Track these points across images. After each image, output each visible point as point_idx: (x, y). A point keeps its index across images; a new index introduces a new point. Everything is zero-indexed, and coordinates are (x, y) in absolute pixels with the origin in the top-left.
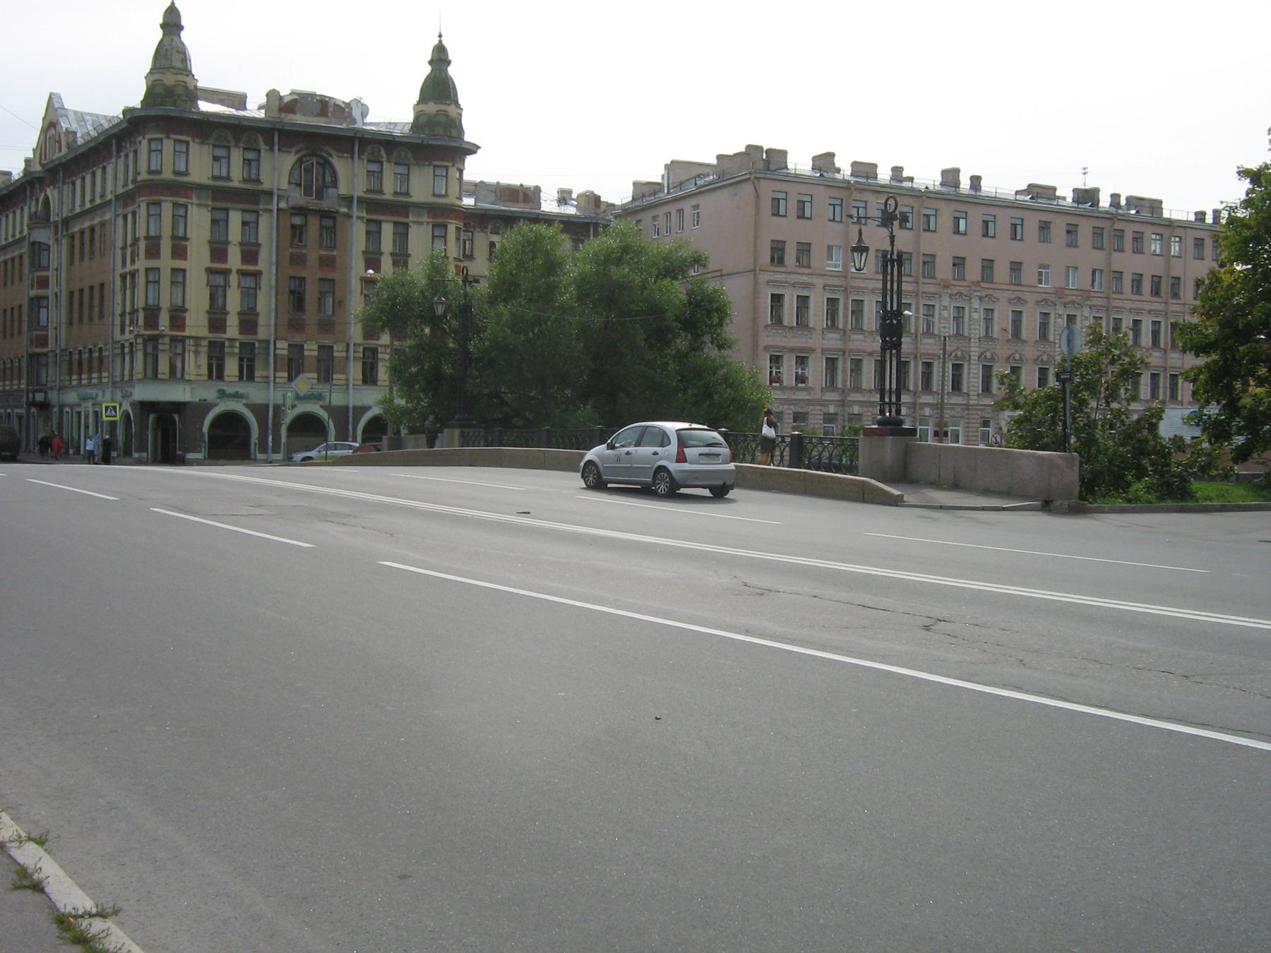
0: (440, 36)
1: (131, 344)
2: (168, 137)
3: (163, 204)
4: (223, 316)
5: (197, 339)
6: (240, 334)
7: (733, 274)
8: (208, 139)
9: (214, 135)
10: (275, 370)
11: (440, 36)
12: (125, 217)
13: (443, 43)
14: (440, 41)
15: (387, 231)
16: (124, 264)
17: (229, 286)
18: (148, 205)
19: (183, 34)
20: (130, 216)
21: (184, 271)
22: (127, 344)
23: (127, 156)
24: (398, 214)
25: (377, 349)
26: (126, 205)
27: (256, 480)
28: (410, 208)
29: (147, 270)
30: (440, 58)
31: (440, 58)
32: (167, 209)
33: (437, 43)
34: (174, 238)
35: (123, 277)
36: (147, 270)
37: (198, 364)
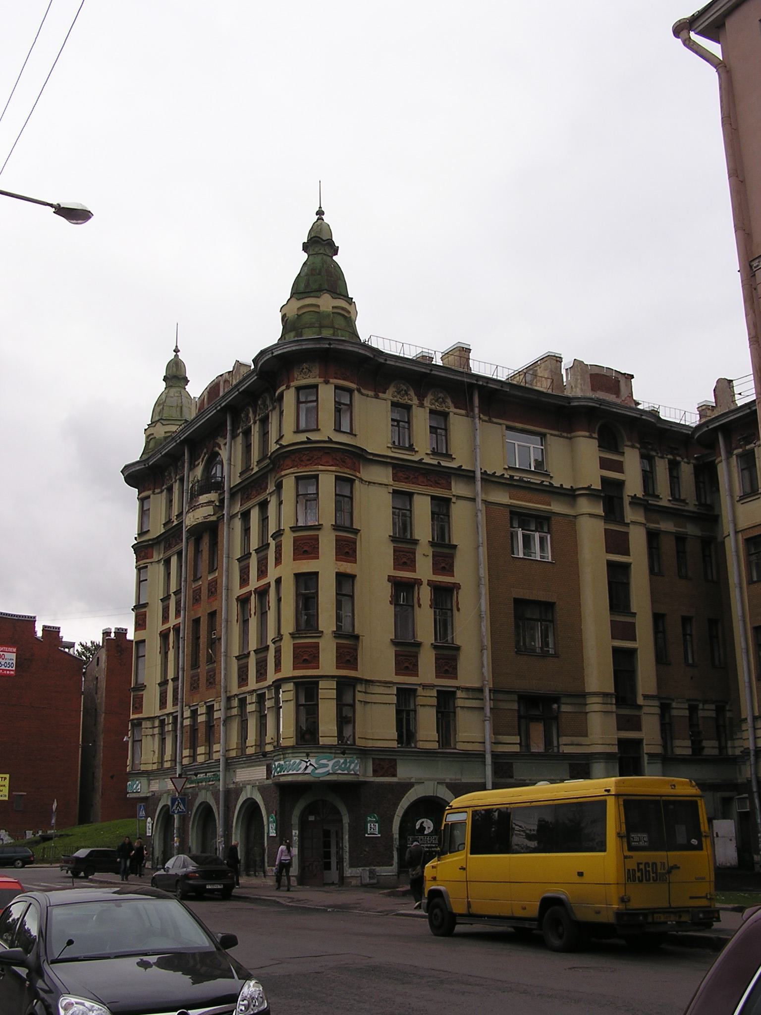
0: (176, 351)
2: (327, 382)
3: (322, 477)
4: (453, 653)
9: (391, 390)
12: (246, 516)
14: (177, 356)
16: (244, 581)
17: (420, 606)
18: (298, 479)
20: (255, 514)
21: (353, 577)
23: (247, 433)
24: (437, 484)
26: (246, 499)
28: (453, 478)
32: (327, 483)
35: (244, 601)
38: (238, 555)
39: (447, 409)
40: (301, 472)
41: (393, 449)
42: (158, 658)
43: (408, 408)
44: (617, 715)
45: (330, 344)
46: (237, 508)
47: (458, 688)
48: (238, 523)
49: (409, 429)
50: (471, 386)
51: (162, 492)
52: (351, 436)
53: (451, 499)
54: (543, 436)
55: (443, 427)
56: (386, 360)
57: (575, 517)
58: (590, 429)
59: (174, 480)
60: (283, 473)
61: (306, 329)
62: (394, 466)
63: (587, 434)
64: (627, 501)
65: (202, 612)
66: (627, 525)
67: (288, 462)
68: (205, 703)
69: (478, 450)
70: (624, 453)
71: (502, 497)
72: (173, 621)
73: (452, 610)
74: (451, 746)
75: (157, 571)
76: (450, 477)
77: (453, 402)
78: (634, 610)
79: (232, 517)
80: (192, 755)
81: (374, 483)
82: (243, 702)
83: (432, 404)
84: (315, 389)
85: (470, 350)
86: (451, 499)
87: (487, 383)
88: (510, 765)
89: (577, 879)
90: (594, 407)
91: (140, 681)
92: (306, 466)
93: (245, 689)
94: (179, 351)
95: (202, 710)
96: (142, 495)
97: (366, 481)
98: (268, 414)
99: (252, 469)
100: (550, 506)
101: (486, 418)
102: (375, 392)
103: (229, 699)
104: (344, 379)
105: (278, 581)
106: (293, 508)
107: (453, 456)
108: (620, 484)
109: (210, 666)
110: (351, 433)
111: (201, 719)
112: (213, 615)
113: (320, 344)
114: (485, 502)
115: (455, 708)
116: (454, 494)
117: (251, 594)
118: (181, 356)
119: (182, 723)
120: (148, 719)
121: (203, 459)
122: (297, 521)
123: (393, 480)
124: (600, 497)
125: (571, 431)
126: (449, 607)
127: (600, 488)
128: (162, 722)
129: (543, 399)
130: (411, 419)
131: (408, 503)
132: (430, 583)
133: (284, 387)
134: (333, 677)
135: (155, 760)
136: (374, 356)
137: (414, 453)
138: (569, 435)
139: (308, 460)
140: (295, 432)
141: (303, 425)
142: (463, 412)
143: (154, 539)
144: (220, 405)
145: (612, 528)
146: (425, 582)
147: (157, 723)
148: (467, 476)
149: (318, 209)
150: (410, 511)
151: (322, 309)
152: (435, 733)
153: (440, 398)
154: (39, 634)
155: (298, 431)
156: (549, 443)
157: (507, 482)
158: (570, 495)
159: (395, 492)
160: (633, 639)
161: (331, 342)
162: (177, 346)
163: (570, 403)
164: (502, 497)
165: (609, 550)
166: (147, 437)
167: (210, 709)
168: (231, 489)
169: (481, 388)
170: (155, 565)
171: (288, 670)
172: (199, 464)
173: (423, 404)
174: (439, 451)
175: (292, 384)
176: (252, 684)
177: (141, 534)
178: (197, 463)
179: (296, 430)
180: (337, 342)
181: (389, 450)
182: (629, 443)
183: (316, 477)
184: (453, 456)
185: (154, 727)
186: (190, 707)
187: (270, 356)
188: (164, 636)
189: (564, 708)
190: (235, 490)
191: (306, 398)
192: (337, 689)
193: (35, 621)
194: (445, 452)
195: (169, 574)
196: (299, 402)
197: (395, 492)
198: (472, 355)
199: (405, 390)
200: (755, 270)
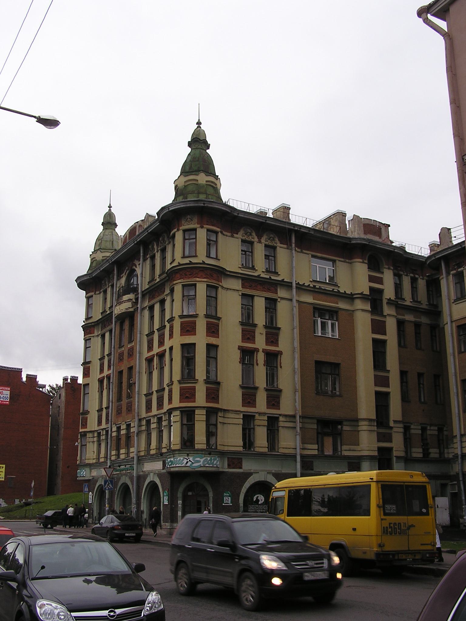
0: (110, 207)
2: (202, 227)
3: (198, 285)
4: (252, 391)
6: (267, 408)
8: (136, 565)
9: (242, 232)
10: (341, 445)
11: (110, 207)
12: (151, 308)
13: (112, 211)
14: (110, 210)
15: (260, 304)
16: (150, 348)
17: (257, 364)
18: (184, 286)
20: (157, 307)
21: (217, 347)
23: (153, 258)
24: (269, 290)
27: (199, 564)
32: (201, 289)
33: (108, 211)
35: (150, 360)
41: (242, 269)
42: (97, 395)
45: (204, 204)
46: (146, 304)
47: (280, 415)
48: (146, 313)
50: (290, 230)
51: (100, 293)
54: (334, 261)
57: (353, 311)
59: (107, 286)
60: (175, 282)
61: (190, 195)
62: (243, 279)
63: (361, 260)
64: (385, 302)
65: (124, 367)
66: (385, 316)
67: (178, 275)
68: (126, 422)
70: (383, 272)
71: (308, 299)
72: (106, 372)
73: (277, 367)
75: (97, 342)
76: (277, 286)
77: (279, 240)
79: (143, 309)
81: (230, 289)
82: (148, 422)
84: (195, 232)
85: (290, 208)
86: (277, 299)
87: (300, 228)
89: (353, 533)
91: (86, 409)
94: (111, 207)
95: (124, 427)
97: (225, 288)
98: (155, 254)
99: (156, 280)
101: (299, 250)
103: (140, 420)
104: (213, 225)
107: (279, 273)
108: (381, 292)
110: (217, 258)
111: (123, 432)
112: (131, 369)
113: (198, 203)
115: (278, 427)
116: (279, 296)
117: (154, 356)
118: (113, 210)
120: (90, 432)
125: (351, 258)
127: (368, 294)
128: (99, 434)
129: (335, 239)
132: (264, 351)
133: (176, 230)
134: (204, 407)
135: (95, 457)
139: (190, 275)
140: (182, 258)
141: (187, 253)
142: (285, 246)
143: (95, 322)
146: (261, 350)
147: (96, 435)
148: (287, 285)
149: (197, 121)
150: (252, 306)
154: (24, 379)
155: (184, 257)
156: (337, 265)
158: (350, 298)
159: (243, 295)
160: (388, 386)
161: (205, 203)
162: (110, 204)
163: (351, 241)
164: (308, 299)
167: (128, 426)
169: (296, 232)
170: (96, 338)
171: (176, 403)
175: (181, 228)
176: (154, 411)
178: (122, 276)
182: (387, 267)
183: (195, 285)
184: (279, 273)
187: (168, 210)
191: (189, 236)
192: (206, 415)
193: (22, 371)
194: (274, 271)
195: (104, 343)
196: (185, 239)
197: (243, 295)
199: (250, 233)
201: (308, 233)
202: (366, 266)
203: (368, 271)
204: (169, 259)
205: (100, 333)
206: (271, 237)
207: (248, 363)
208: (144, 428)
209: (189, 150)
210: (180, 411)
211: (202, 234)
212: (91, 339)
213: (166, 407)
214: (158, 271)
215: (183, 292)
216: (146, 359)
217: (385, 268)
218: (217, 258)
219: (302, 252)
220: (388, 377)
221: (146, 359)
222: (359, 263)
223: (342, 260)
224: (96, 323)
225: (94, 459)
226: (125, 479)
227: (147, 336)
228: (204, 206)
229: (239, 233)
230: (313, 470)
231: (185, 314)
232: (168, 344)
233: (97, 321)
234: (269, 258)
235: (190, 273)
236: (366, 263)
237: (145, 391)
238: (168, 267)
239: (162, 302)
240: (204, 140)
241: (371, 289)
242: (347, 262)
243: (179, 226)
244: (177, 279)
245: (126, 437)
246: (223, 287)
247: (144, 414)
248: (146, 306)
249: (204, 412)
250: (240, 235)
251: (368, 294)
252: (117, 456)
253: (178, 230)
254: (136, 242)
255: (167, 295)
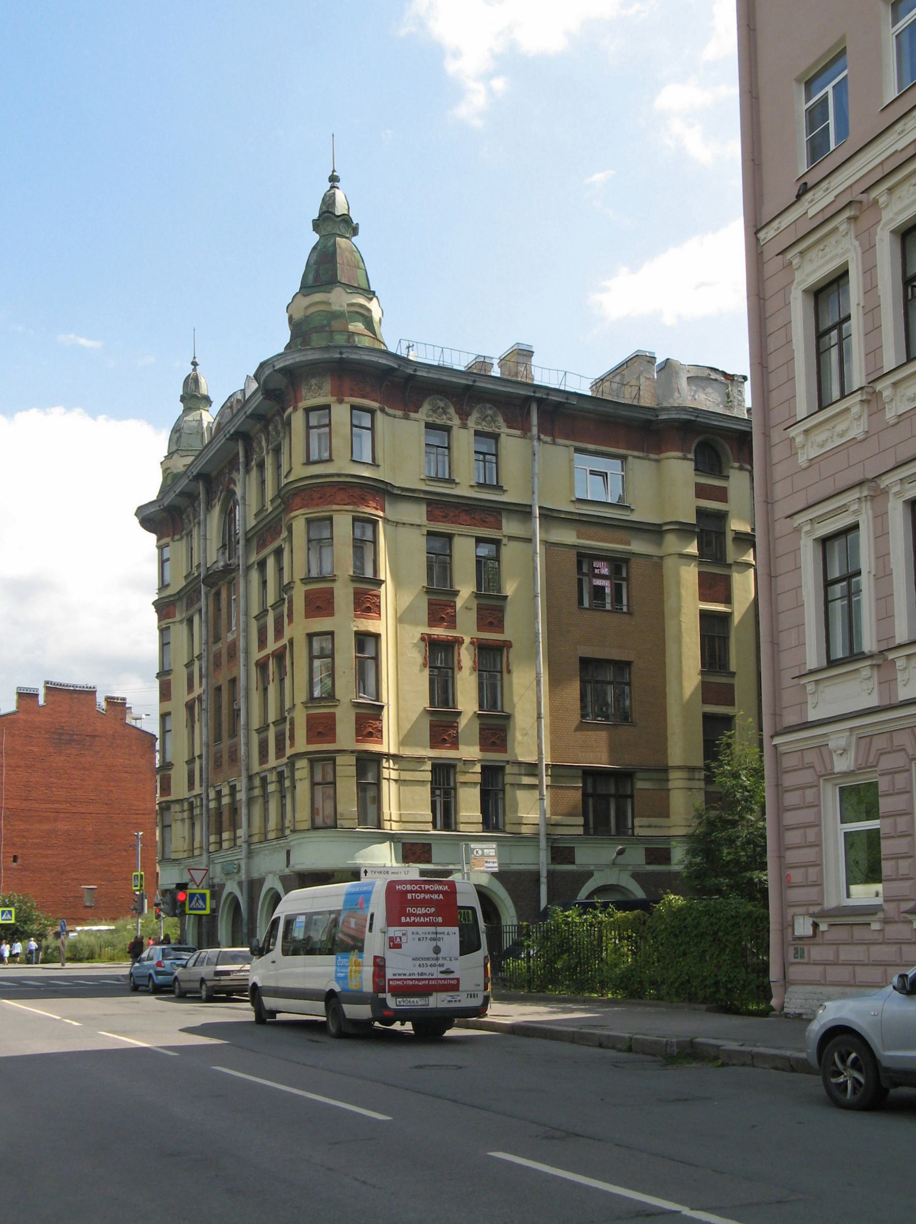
1: (281, 775)
2: (341, 401)
3: (336, 518)
4: (450, 719)
5: (532, 769)
7: (321, 562)
9: (426, 408)
11: (195, 358)
12: (262, 565)
16: (262, 643)
17: (460, 668)
18: (309, 521)
19: (158, 671)
22: (272, 777)
23: (261, 466)
24: (483, 523)
25: (454, 766)
26: (262, 546)
28: (504, 514)
29: (310, 636)
30: (181, 1030)
31: (181, 1030)
32: (343, 525)
34: (358, 578)
35: (262, 666)
36: (310, 636)
37: (178, 435)
38: (196, 564)
39: (497, 430)
40: (312, 513)
41: (428, 482)
42: (185, 732)
43: (448, 429)
44: (706, 793)
45: (341, 353)
46: (254, 558)
47: (508, 762)
48: (255, 575)
49: (449, 456)
50: (527, 400)
51: (182, 538)
52: (373, 468)
53: (501, 540)
54: (623, 458)
55: (494, 453)
56: (415, 370)
57: (662, 558)
58: (684, 449)
59: (192, 524)
60: (293, 514)
62: (429, 503)
63: (680, 454)
64: (729, 537)
65: (222, 679)
66: (730, 566)
67: (297, 500)
68: (229, 782)
69: (536, 480)
70: (728, 477)
71: (568, 536)
72: (198, 691)
73: (501, 672)
74: (610, 831)
75: (179, 632)
76: (500, 514)
77: (505, 421)
78: (733, 667)
79: (248, 568)
80: (218, 841)
81: (404, 524)
82: (264, 782)
83: (478, 423)
84: (327, 411)
85: (533, 352)
86: (501, 540)
87: (548, 394)
88: (572, 850)
90: (689, 420)
91: (168, 759)
92: (317, 505)
93: (266, 766)
95: (226, 791)
96: (159, 543)
97: (393, 522)
99: (267, 509)
100: (630, 545)
101: (548, 439)
102: (405, 411)
103: (250, 778)
104: (363, 397)
105: (291, 642)
106: (304, 556)
107: (504, 488)
108: (721, 517)
109: (232, 741)
110: (374, 464)
111: (225, 800)
112: (233, 682)
114: (545, 542)
115: (504, 785)
116: (505, 534)
117: (269, 658)
119: (207, 806)
120: (177, 801)
121: (219, 499)
122: (309, 571)
123: (428, 520)
124: (693, 532)
125: (660, 451)
126: (499, 669)
127: (694, 522)
128: (191, 807)
129: (623, 413)
130: (451, 444)
131: (448, 547)
133: (290, 410)
134: (352, 752)
135: (186, 848)
136: (400, 366)
137: (454, 486)
138: (656, 457)
139: (321, 498)
140: (304, 464)
141: (314, 456)
142: (518, 432)
143: (174, 595)
144: (228, 432)
145: (713, 571)
146: (467, 640)
147: (186, 806)
148: (523, 512)
149: (331, 173)
150: (450, 556)
151: (335, 308)
152: (430, 812)
153: (487, 416)
154: (104, 704)
156: (630, 467)
157: (574, 518)
158: (655, 532)
159: (430, 534)
160: (731, 703)
161: (343, 351)
163: (657, 416)
164: (568, 536)
165: (703, 598)
166: (164, 471)
167: (233, 789)
168: (246, 533)
169: (540, 401)
170: (178, 626)
171: (301, 744)
172: (215, 505)
173: (466, 424)
174: (487, 483)
176: (272, 761)
177: (163, 586)
178: (213, 503)
179: (305, 461)
180: (349, 350)
181: (423, 483)
182: (736, 465)
183: (330, 519)
184: (504, 488)
185: (184, 811)
186: (215, 787)
187: (271, 370)
188: (190, 707)
189: (639, 785)
190: (250, 535)
192: (357, 765)
193: (96, 691)
194: (495, 483)
195: (192, 635)
196: (308, 428)
197: (430, 534)
198: (535, 360)
199: (443, 408)
200: (762, 244)
201: (564, 403)
202: (691, 465)
203: (696, 475)
204: (285, 469)
205: (184, 615)
206: (487, 416)
207: (443, 665)
208: (257, 792)
209: (316, 238)
210: (309, 759)
211: (341, 414)
212: (169, 627)
213: (289, 752)
214: (270, 493)
215: (308, 532)
216: (258, 664)
217: (732, 468)
218: (374, 464)
219: (554, 443)
220: (732, 686)
221: (258, 664)
222: (676, 460)
223: (641, 454)
224: (177, 597)
225: (185, 851)
226: (231, 887)
227: (257, 620)
228: (341, 359)
229: (420, 409)
230: (573, 863)
231: (314, 574)
232: (288, 632)
233: (179, 593)
234: (484, 457)
235: (319, 495)
236: (691, 460)
237: (256, 723)
238: (284, 482)
239: (279, 552)
240: (344, 215)
241: (701, 513)
242: (650, 459)
243: (296, 402)
244: (297, 508)
245: (230, 808)
246: (389, 520)
247: (256, 768)
248: (254, 562)
249: (352, 760)
250: (423, 414)
251: (694, 522)
252: (232, 843)
253: (295, 409)
254: (228, 436)
255: (284, 539)
